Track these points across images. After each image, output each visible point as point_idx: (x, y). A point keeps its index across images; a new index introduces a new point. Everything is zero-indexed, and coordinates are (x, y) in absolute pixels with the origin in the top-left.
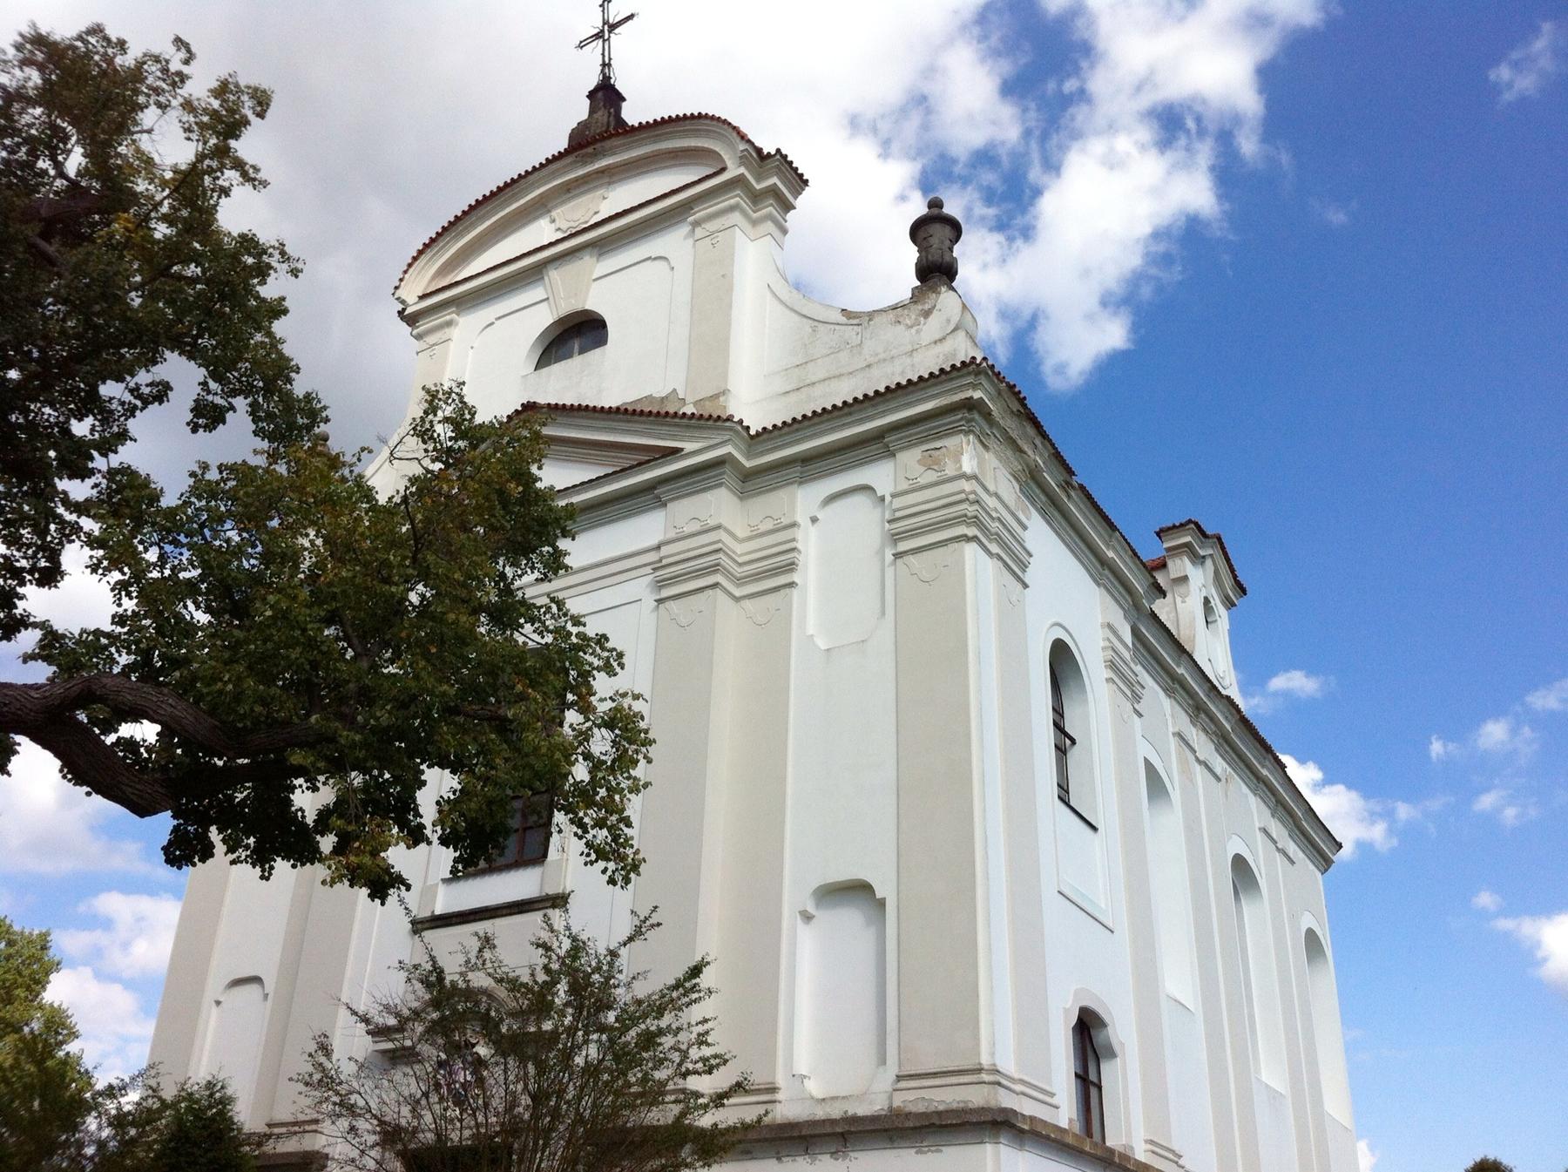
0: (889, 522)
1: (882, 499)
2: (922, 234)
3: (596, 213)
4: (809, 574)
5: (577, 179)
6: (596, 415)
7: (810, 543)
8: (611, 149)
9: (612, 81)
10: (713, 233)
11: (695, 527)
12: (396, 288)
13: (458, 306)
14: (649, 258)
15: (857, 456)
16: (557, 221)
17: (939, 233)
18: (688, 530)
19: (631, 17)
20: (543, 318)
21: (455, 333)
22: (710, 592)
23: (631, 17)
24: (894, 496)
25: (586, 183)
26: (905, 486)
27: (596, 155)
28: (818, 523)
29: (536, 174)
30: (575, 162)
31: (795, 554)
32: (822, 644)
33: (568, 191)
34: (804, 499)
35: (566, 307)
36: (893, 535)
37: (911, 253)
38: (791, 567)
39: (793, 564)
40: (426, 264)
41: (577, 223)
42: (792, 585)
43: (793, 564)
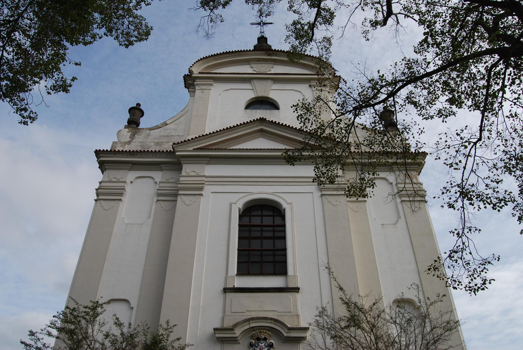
0: (157, 189)
1: (156, 183)
2: (132, 111)
3: (270, 71)
4: (126, 199)
5: (263, 59)
6: (225, 131)
7: (128, 188)
8: (279, 55)
9: (265, 36)
10: (202, 89)
11: (194, 174)
12: (191, 67)
13: (274, 81)
14: (294, 90)
15: (381, 168)
16: (254, 68)
17: (138, 113)
18: (191, 174)
19: (271, 23)
20: (250, 95)
21: (212, 88)
22: (199, 196)
23: (271, 23)
24: (160, 182)
25: (266, 61)
26: (164, 180)
27: (273, 55)
28: (132, 183)
29: (247, 52)
30: (265, 54)
31: (124, 191)
32: (126, 221)
33: (259, 61)
34: (131, 175)
35: (261, 94)
36: (158, 194)
37: (128, 116)
38: (121, 194)
39: (122, 193)
40: (202, 64)
41: (263, 71)
42: (120, 200)
43: (122, 193)
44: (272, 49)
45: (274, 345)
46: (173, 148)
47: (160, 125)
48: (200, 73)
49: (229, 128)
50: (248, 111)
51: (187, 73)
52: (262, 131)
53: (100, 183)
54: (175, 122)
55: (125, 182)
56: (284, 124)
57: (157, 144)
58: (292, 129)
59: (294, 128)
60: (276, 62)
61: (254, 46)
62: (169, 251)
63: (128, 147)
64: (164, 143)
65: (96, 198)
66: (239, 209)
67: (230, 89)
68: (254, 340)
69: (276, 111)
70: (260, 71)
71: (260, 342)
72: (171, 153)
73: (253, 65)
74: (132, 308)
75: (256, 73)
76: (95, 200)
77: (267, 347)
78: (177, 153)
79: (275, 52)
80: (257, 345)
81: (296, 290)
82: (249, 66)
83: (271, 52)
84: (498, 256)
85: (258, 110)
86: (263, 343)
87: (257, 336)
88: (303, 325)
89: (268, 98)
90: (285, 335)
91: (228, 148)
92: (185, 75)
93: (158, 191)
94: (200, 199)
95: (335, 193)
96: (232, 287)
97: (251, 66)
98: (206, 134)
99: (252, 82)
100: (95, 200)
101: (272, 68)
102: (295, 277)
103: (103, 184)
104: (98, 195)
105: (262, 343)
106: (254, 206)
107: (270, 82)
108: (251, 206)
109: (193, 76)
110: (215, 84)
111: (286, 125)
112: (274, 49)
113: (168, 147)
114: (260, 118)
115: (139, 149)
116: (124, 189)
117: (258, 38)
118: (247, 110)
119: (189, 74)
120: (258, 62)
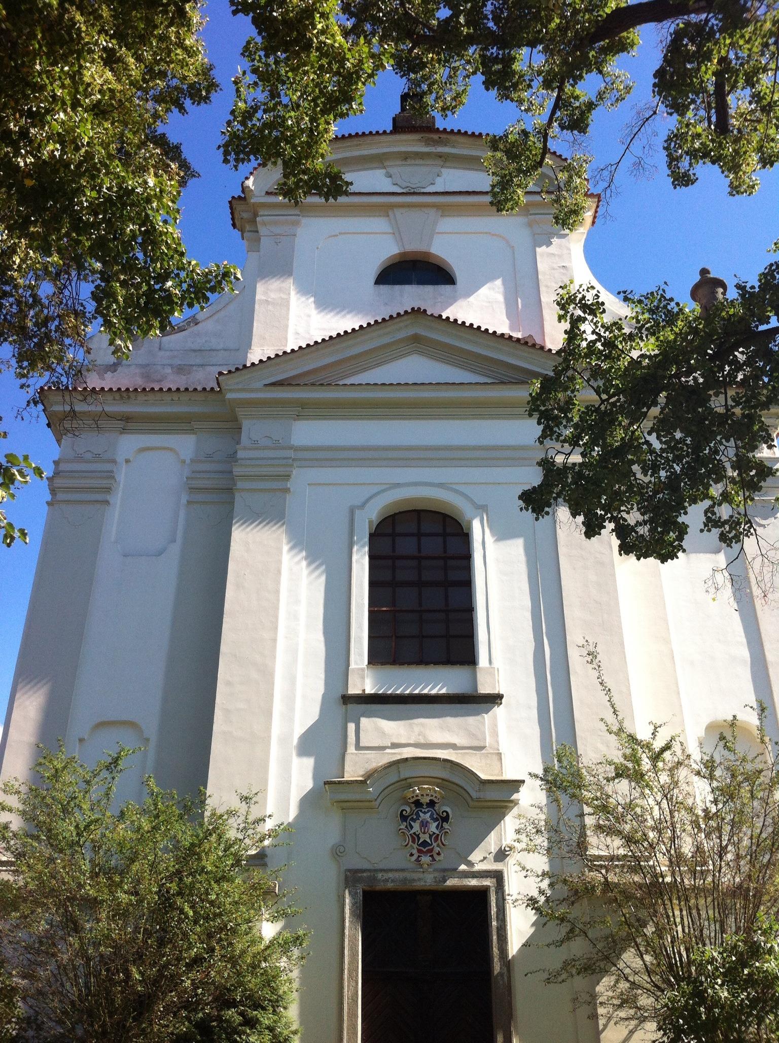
31: (113, 482)
35: (414, 246)
38: (108, 490)
39: (110, 488)
43: (110, 488)
44: (438, 129)
45: (451, 816)
46: (218, 384)
47: (181, 324)
48: (268, 193)
49: (342, 334)
50: (384, 289)
51: (238, 193)
52: (416, 339)
53: (56, 463)
54: (216, 317)
55: (114, 462)
56: (467, 324)
57: (180, 370)
58: (485, 336)
59: (491, 331)
60: (446, 160)
61: (394, 120)
62: (543, 324)
63: (113, 377)
64: (194, 368)
65: (49, 497)
66: (370, 522)
67: (340, 233)
68: (409, 806)
69: (448, 288)
70: (409, 185)
71: (421, 811)
72: (213, 393)
73: (392, 171)
74: (148, 740)
75: (399, 190)
76: (48, 503)
77: (435, 820)
78: (229, 396)
79: (443, 136)
80: (415, 817)
81: (495, 699)
82: (384, 171)
83: (435, 136)
84: (524, 511)
85: (407, 286)
86: (428, 811)
87: (416, 798)
88: (509, 775)
89: (428, 254)
90: (474, 795)
91: (341, 383)
92: (233, 197)
93: (189, 482)
94: (285, 499)
95: (258, 462)
96: (360, 692)
97: (387, 172)
98: (293, 350)
99: (390, 213)
100: (48, 503)
101: (438, 176)
102: (491, 671)
103: (63, 467)
104: (53, 491)
105: (425, 813)
106: (400, 513)
107: (432, 212)
108: (395, 514)
109: (252, 201)
110: (304, 221)
111: (472, 325)
112: (441, 129)
113: (204, 378)
114: (413, 309)
115: (139, 382)
116: (113, 477)
117: (401, 96)
118: (381, 287)
119: (243, 196)
120: (404, 163)
